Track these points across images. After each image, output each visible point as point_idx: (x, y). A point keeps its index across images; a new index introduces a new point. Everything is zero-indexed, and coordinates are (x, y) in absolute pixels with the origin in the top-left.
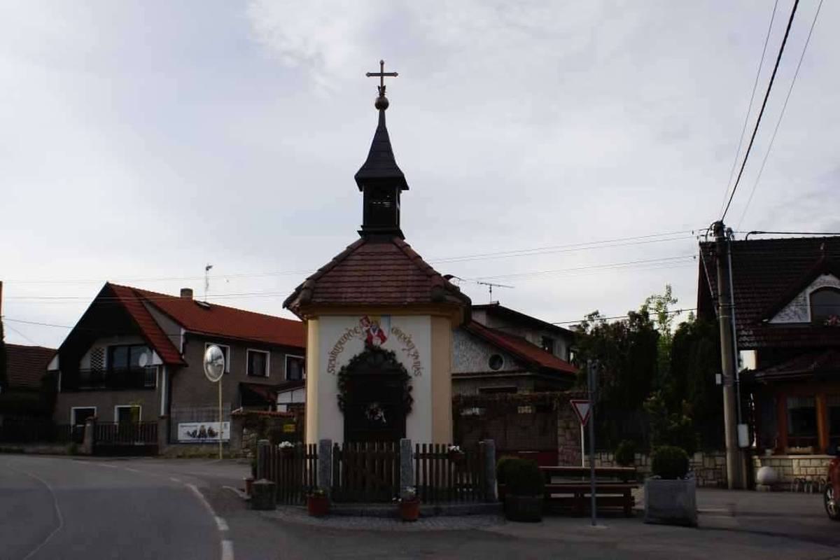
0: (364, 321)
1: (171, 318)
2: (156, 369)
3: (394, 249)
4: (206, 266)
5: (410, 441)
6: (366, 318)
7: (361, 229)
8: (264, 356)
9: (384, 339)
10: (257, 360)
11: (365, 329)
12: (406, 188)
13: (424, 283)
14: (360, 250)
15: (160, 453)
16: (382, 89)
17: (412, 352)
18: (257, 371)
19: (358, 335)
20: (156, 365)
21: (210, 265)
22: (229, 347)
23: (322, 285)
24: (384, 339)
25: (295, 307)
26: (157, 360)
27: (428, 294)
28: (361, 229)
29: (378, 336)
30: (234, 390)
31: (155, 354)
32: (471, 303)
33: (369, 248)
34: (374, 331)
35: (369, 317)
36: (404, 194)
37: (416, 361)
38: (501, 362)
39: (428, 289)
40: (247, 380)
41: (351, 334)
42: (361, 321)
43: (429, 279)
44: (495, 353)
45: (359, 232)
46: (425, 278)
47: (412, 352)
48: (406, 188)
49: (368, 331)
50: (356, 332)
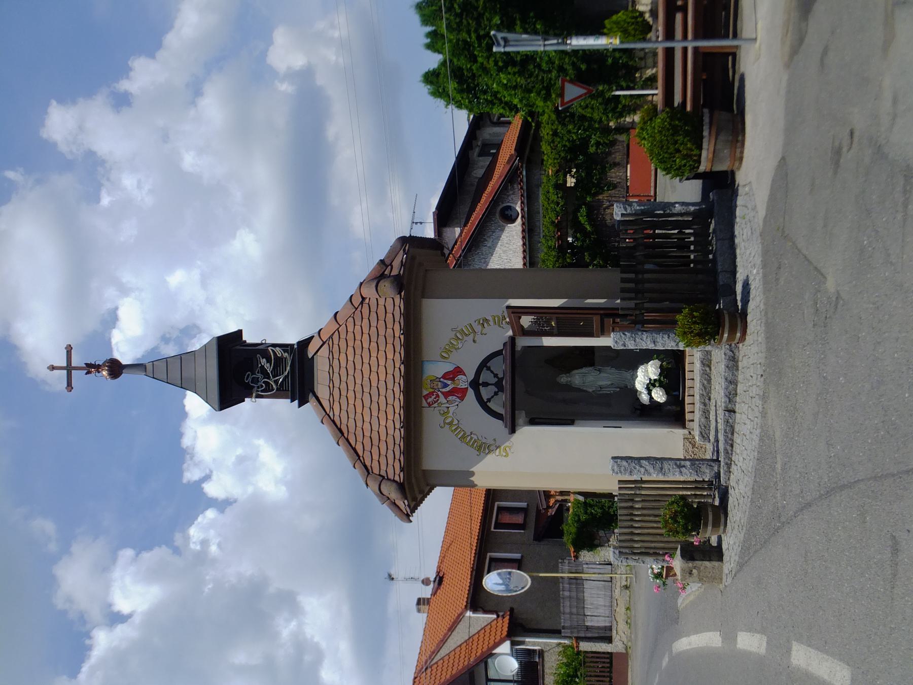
0: (430, 400)
1: (452, 628)
2: (517, 650)
3: (325, 351)
4: (388, 581)
5: (624, 657)
6: (426, 397)
7: (296, 402)
8: (500, 509)
9: (458, 371)
10: (507, 518)
11: (442, 399)
12: (239, 333)
13: (373, 309)
14: (326, 404)
15: (624, 651)
16: (91, 368)
17: (478, 328)
18: (519, 519)
19: (451, 410)
20: (512, 649)
21: (387, 576)
22: (489, 554)
23: (375, 464)
24: (458, 371)
25: (409, 506)
26: (505, 647)
27: (390, 301)
28: (296, 402)
29: (453, 379)
30: (544, 548)
31: (496, 651)
32: (61, 101)
33: (322, 390)
34: (446, 385)
35: (425, 393)
36: (248, 338)
37: (491, 323)
38: (509, 208)
39: (382, 301)
40: (530, 532)
41: (448, 421)
42: (430, 405)
43: (367, 301)
44: (497, 215)
45: (300, 405)
46: (366, 306)
47: (478, 328)
48: (239, 333)
49: (446, 395)
50: (448, 412)
